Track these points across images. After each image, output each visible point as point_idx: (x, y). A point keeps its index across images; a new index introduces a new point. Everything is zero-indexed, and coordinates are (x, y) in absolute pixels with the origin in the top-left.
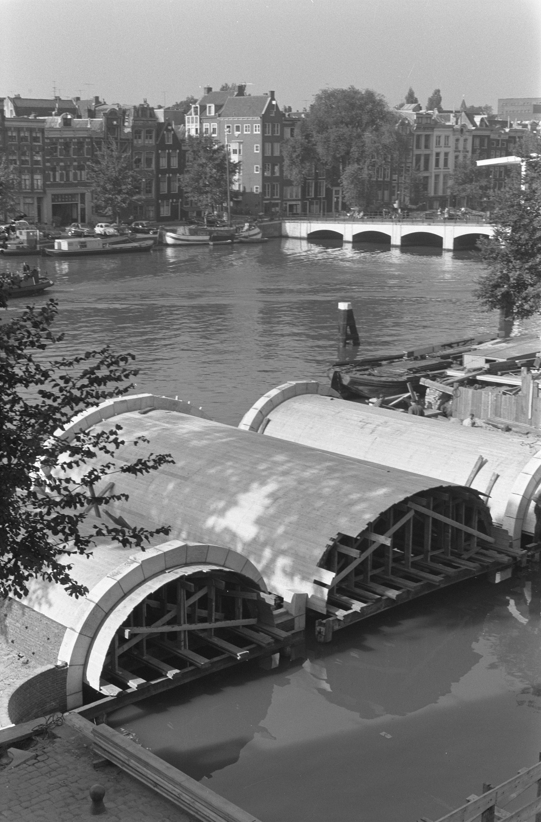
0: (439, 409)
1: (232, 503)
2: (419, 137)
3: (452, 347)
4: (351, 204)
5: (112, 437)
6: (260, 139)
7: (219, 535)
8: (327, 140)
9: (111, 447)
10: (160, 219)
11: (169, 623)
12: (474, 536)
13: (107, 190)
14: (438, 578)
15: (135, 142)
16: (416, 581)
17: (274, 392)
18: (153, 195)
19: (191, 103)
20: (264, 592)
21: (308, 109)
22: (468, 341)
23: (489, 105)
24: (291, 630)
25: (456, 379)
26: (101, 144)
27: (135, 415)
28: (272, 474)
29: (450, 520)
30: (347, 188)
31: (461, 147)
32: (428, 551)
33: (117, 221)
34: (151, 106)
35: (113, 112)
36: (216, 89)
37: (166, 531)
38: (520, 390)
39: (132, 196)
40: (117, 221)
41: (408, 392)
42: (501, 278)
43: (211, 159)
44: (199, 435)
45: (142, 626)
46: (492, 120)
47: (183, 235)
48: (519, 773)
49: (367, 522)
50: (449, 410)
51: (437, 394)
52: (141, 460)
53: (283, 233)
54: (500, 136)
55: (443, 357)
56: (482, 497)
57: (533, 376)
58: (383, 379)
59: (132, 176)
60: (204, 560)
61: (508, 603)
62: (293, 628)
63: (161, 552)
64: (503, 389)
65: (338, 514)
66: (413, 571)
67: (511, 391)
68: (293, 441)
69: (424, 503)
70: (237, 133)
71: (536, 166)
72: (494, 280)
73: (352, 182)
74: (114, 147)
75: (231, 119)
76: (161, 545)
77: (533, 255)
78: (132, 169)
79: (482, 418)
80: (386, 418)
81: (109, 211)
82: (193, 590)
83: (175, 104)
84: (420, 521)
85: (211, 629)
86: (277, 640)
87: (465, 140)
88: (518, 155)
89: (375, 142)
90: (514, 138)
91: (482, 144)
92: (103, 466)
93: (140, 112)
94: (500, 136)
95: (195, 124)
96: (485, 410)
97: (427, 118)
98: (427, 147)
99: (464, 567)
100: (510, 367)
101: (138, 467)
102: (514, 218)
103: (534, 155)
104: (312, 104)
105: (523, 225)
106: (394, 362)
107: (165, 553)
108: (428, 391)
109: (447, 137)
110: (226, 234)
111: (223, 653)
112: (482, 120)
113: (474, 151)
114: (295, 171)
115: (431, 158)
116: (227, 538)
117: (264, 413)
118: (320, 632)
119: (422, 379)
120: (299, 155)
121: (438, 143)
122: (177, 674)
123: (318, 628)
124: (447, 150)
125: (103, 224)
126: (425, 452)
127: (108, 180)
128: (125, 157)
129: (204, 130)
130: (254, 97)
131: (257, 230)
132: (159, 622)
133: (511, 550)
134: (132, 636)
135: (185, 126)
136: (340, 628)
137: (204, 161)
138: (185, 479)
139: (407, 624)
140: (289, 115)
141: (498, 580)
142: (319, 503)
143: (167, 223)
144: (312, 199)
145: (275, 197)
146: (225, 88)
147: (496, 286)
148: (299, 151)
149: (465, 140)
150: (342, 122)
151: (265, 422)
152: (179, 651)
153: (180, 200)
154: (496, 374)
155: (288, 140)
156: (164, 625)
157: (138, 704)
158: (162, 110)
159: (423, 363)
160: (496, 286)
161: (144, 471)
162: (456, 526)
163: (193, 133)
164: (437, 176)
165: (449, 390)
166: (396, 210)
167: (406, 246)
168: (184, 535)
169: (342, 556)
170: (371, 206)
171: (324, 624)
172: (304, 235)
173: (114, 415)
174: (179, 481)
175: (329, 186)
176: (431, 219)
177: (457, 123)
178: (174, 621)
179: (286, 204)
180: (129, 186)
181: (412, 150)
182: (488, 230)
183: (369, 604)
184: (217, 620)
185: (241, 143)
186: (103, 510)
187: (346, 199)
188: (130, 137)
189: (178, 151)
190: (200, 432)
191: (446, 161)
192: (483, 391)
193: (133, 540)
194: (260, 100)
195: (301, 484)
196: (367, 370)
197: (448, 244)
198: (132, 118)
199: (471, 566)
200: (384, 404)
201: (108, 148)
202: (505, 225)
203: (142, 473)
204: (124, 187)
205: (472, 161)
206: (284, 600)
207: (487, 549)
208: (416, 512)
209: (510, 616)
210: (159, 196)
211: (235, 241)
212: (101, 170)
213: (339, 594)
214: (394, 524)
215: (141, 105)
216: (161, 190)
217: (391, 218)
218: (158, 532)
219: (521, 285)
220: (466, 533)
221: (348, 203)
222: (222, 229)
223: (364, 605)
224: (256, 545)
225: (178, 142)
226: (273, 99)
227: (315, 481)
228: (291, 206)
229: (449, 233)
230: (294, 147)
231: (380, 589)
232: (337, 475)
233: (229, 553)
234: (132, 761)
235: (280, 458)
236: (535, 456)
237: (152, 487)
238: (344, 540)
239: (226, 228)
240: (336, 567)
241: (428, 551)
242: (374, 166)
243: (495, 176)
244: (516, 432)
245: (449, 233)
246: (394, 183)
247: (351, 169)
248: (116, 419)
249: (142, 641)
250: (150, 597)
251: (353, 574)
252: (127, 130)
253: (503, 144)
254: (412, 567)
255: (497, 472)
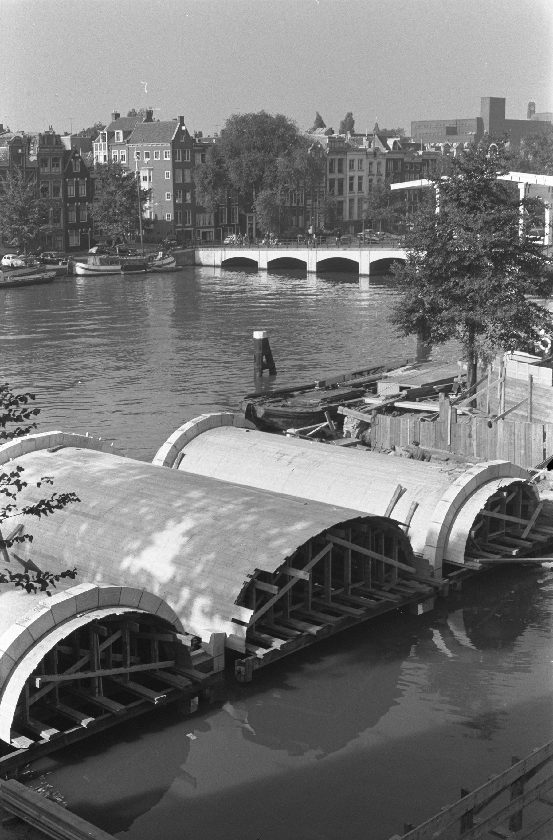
0: (357, 437)
1: (148, 543)
2: (333, 160)
3: (363, 375)
4: (264, 230)
5: (14, 479)
6: (170, 165)
7: (135, 576)
8: (240, 165)
9: (13, 489)
10: (69, 250)
11: (83, 669)
12: (395, 567)
13: (13, 221)
14: (359, 612)
15: (41, 170)
16: (337, 615)
17: (188, 426)
18: (61, 225)
19: (99, 129)
20: (180, 633)
21: (219, 134)
22: (378, 368)
23: (401, 128)
24: (210, 671)
25: (374, 407)
26: (6, 173)
27: (44, 453)
28: (188, 511)
29: (370, 551)
30: (259, 216)
31: (375, 171)
32: (349, 585)
33: (25, 252)
34: (56, 133)
35: (17, 139)
36: (124, 115)
37: (71, 574)
38: (438, 416)
39: (40, 226)
40: (25, 252)
41: (326, 421)
42: (415, 302)
43: (120, 186)
44: (112, 473)
45: (54, 674)
46: (405, 143)
47: (93, 265)
48: (442, 810)
49: (285, 557)
50: (368, 438)
51: (356, 422)
52: (45, 500)
53: (197, 261)
54: (413, 159)
55: (354, 386)
56: (401, 527)
57: (450, 402)
58: (298, 410)
59: (40, 206)
60: (117, 603)
61: (432, 635)
62: (212, 669)
63: (73, 596)
64: (422, 416)
65: (256, 549)
66: (333, 605)
67: (429, 417)
68: (209, 475)
69: (343, 535)
70: (147, 160)
71: (447, 189)
72: (409, 305)
73: (265, 208)
74: (19, 176)
75: (140, 145)
76: (71, 589)
77: (447, 279)
78: (39, 198)
79: (401, 445)
80: (303, 449)
81: (15, 241)
82: (106, 634)
83: (82, 130)
84: (339, 554)
85: (126, 674)
86: (195, 683)
87: (379, 164)
88: (429, 178)
89: (287, 167)
90: (427, 160)
91: (395, 167)
92: (3, 508)
93: (46, 140)
94: (413, 159)
95: (103, 151)
96: (403, 438)
97: (340, 141)
98: (340, 171)
99: (384, 600)
100: (427, 393)
101: (41, 508)
102: (427, 241)
103: (445, 178)
104: (223, 128)
105: (436, 249)
106: (305, 392)
107: (75, 597)
108: (346, 419)
109: (360, 161)
110: (138, 263)
111: (140, 699)
112: (395, 143)
113: (387, 175)
114: (207, 198)
115: (344, 182)
116: (143, 579)
117: (177, 447)
118: (239, 672)
119: (340, 408)
120: (211, 181)
121: (352, 167)
122: (91, 722)
123: (237, 668)
124: (360, 174)
125: (10, 256)
126: (343, 482)
127: (15, 209)
128: (32, 186)
129: (113, 157)
130: (163, 123)
131: (171, 259)
132: (72, 669)
133: (432, 579)
134: (42, 684)
135: (93, 153)
136: (260, 666)
137: (113, 188)
138: (96, 518)
139: (330, 661)
140: (199, 141)
141: (420, 610)
142: (237, 540)
143: (77, 253)
144: (226, 226)
145: (187, 225)
146: (132, 114)
147: (412, 311)
148: (210, 176)
149: (379, 164)
150: (254, 147)
151: (179, 456)
152: (93, 698)
153: (90, 229)
154: (415, 401)
155: (199, 166)
156: (77, 671)
157: (51, 755)
158: (69, 137)
159: (335, 393)
160: (412, 311)
161: (48, 511)
162: (376, 558)
163: (101, 160)
164: (351, 201)
165: (367, 418)
166: (310, 235)
167: (321, 272)
168: (99, 577)
169: (260, 592)
170: (286, 232)
171: (244, 663)
172: (219, 263)
173: (22, 454)
174: (91, 520)
175: (243, 212)
176: (345, 244)
177: (370, 147)
178: (87, 667)
179: (199, 231)
180: (36, 216)
181: (326, 174)
182: (401, 254)
183: (289, 641)
184: (132, 664)
185: (151, 169)
186: (12, 554)
187: (259, 225)
188: (36, 165)
189: (86, 179)
190: (112, 470)
191: (360, 185)
192: (401, 418)
193: (38, 585)
194: (169, 126)
195: (218, 520)
196: (280, 401)
197: (364, 269)
198: (37, 146)
199: (393, 598)
200: (303, 435)
201: (14, 177)
202: (418, 248)
203: (46, 514)
204: (30, 217)
205: (386, 185)
206: (202, 640)
207: (408, 580)
208: (335, 544)
209: (435, 648)
210: (68, 226)
211: (148, 270)
212: (6, 200)
213: (257, 633)
214: (313, 557)
215: (46, 132)
216: (70, 219)
217: (306, 244)
218: (64, 575)
219: (435, 310)
220: (386, 564)
221: (261, 229)
222: (135, 258)
223: (285, 642)
224: (174, 586)
225: (86, 170)
226: (182, 124)
227: (232, 517)
228: (204, 234)
229: (364, 258)
230: (205, 173)
231: (302, 625)
232: (253, 510)
233: (142, 593)
234: (43, 817)
235: (195, 494)
236: (454, 483)
237: (64, 529)
238: (261, 576)
239: (139, 257)
240: (255, 604)
241: (349, 585)
242: (287, 190)
243: (409, 200)
244: (436, 459)
245: (364, 258)
246: (309, 208)
247: (264, 194)
248: (20, 461)
249: (53, 690)
250: (61, 643)
251: (273, 610)
252: (33, 158)
253: (416, 167)
254: (332, 601)
255: (416, 501)
